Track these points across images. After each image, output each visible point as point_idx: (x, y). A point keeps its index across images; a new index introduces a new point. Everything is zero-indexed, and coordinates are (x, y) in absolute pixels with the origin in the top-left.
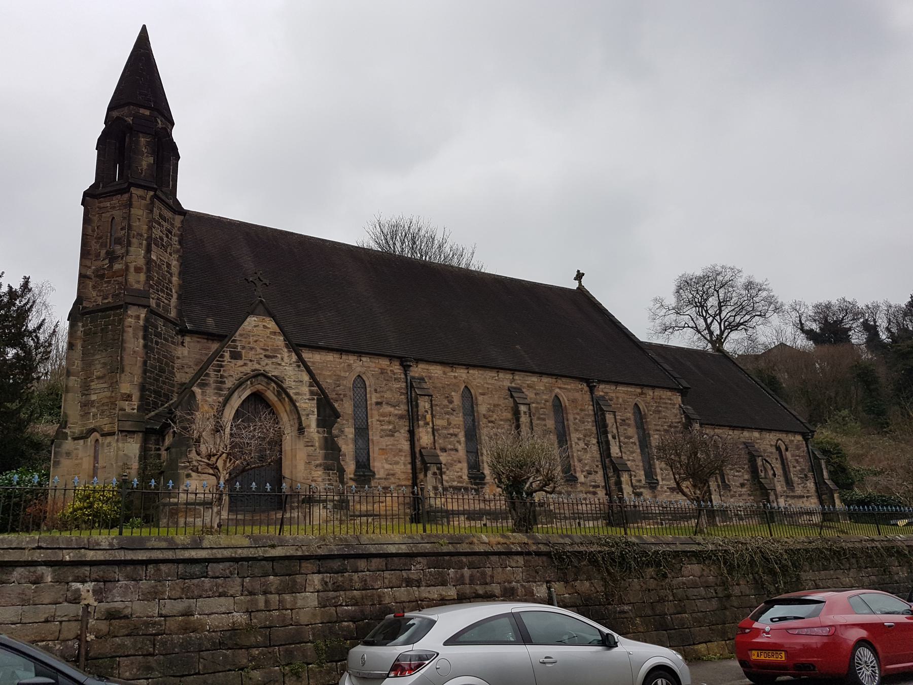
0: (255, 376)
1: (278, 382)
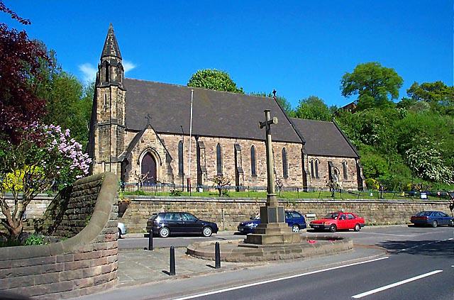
1: (155, 149)
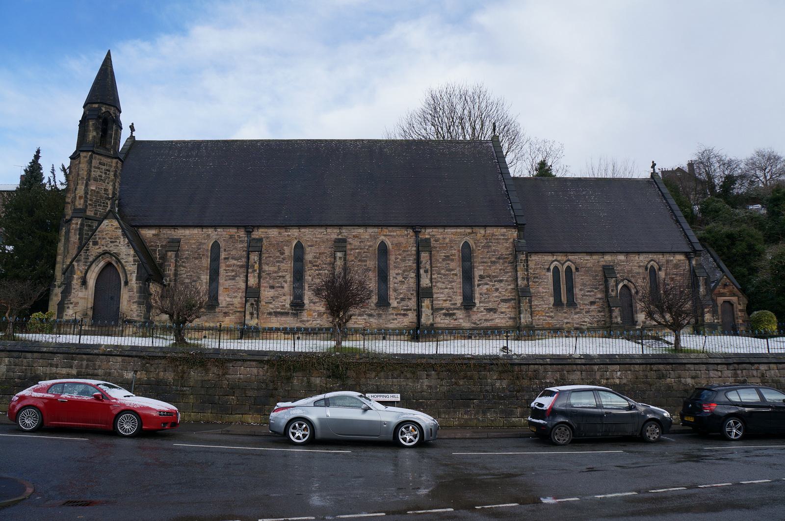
0: (104, 254)
1: (116, 256)
